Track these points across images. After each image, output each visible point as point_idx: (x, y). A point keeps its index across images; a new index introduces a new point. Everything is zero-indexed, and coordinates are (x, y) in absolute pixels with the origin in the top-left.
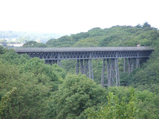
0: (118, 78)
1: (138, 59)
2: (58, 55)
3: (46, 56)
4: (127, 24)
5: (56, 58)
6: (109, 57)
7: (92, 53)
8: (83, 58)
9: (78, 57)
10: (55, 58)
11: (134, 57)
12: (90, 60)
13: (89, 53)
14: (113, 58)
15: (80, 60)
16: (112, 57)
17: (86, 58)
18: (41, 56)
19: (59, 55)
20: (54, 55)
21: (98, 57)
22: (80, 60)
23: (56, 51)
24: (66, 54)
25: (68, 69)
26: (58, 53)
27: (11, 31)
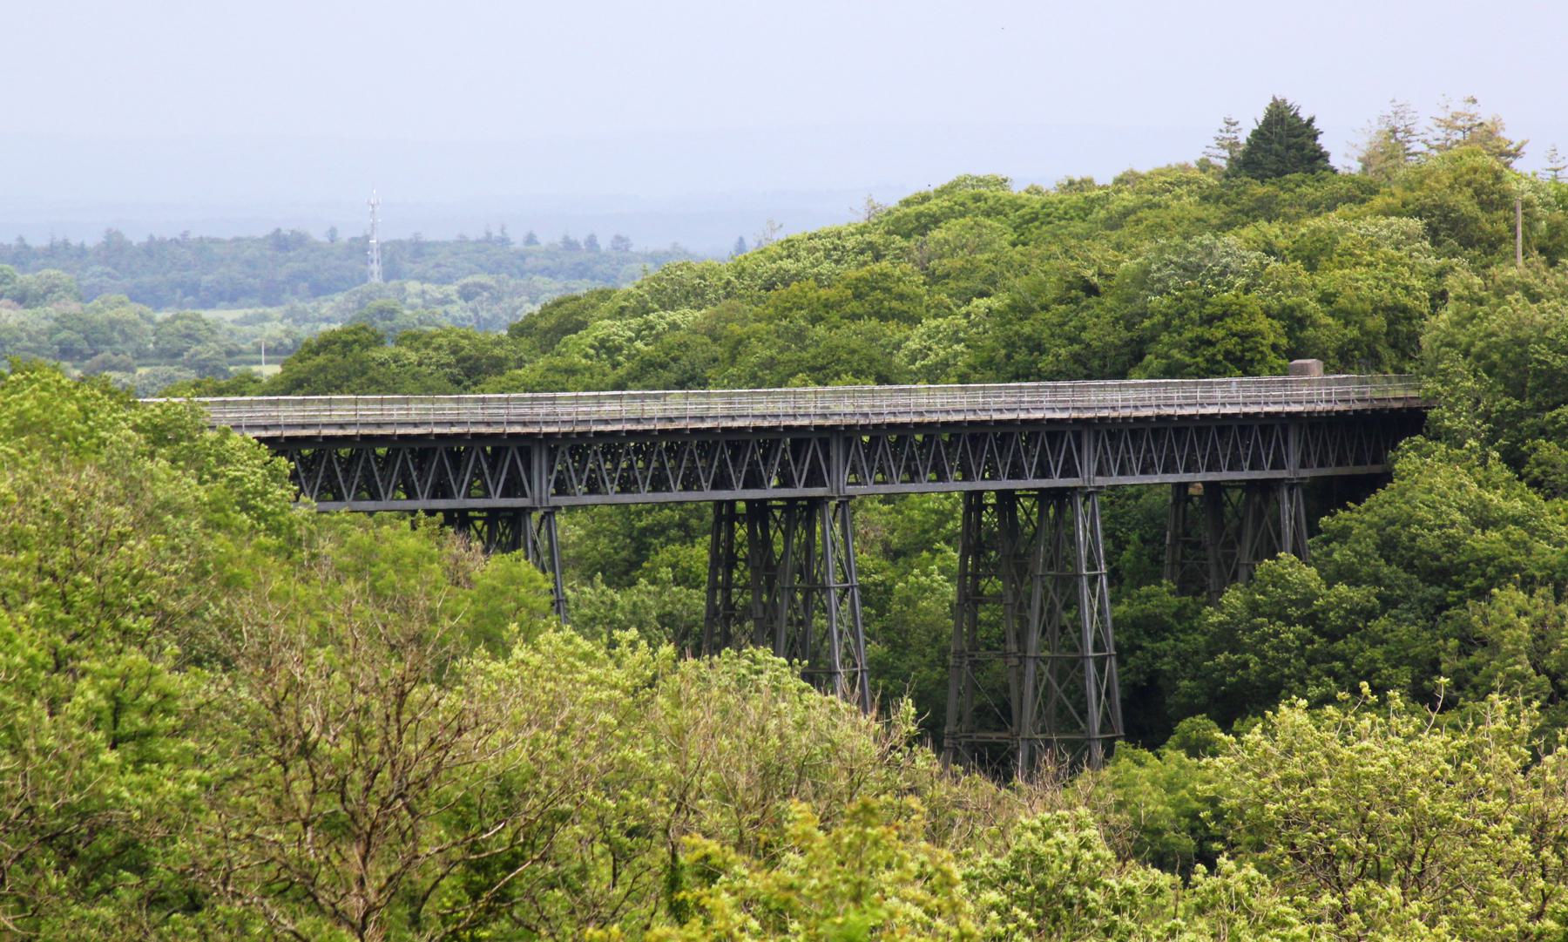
0: (1101, 669)
1: (1298, 492)
2: (528, 468)
3: (419, 468)
4: (397, 238)
5: (814, 479)
6: (1016, 474)
7: (1097, 433)
8: (772, 491)
9: (721, 482)
10: (506, 493)
11: (1256, 475)
12: (833, 503)
13: (825, 445)
14: (1057, 482)
15: (741, 506)
16: (1044, 472)
17: (800, 491)
18: (938, 453)
19: (539, 462)
20: (493, 467)
21: (913, 476)
22: (741, 506)
23: (660, 426)
24: (675, 452)
25: (829, 588)
26: (526, 445)
27: (1083, 181)
